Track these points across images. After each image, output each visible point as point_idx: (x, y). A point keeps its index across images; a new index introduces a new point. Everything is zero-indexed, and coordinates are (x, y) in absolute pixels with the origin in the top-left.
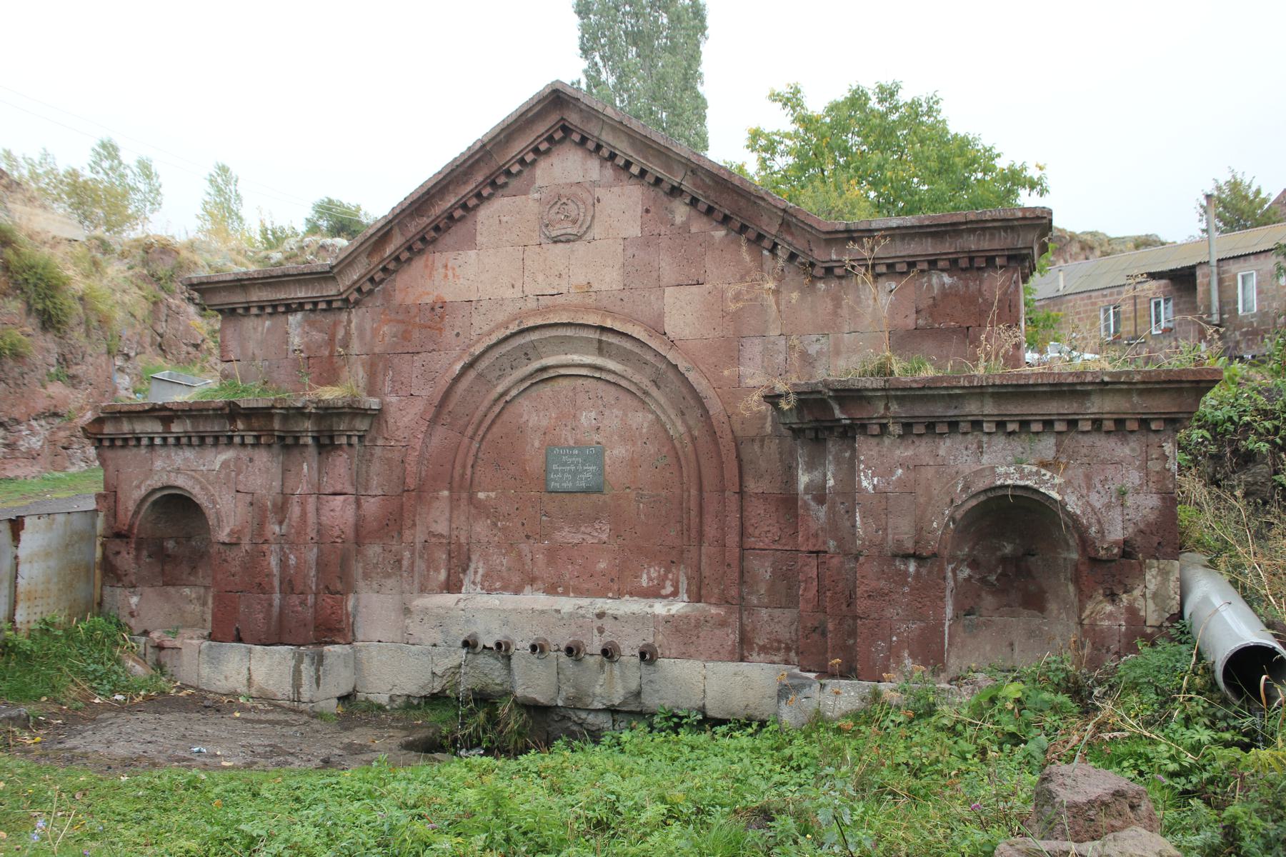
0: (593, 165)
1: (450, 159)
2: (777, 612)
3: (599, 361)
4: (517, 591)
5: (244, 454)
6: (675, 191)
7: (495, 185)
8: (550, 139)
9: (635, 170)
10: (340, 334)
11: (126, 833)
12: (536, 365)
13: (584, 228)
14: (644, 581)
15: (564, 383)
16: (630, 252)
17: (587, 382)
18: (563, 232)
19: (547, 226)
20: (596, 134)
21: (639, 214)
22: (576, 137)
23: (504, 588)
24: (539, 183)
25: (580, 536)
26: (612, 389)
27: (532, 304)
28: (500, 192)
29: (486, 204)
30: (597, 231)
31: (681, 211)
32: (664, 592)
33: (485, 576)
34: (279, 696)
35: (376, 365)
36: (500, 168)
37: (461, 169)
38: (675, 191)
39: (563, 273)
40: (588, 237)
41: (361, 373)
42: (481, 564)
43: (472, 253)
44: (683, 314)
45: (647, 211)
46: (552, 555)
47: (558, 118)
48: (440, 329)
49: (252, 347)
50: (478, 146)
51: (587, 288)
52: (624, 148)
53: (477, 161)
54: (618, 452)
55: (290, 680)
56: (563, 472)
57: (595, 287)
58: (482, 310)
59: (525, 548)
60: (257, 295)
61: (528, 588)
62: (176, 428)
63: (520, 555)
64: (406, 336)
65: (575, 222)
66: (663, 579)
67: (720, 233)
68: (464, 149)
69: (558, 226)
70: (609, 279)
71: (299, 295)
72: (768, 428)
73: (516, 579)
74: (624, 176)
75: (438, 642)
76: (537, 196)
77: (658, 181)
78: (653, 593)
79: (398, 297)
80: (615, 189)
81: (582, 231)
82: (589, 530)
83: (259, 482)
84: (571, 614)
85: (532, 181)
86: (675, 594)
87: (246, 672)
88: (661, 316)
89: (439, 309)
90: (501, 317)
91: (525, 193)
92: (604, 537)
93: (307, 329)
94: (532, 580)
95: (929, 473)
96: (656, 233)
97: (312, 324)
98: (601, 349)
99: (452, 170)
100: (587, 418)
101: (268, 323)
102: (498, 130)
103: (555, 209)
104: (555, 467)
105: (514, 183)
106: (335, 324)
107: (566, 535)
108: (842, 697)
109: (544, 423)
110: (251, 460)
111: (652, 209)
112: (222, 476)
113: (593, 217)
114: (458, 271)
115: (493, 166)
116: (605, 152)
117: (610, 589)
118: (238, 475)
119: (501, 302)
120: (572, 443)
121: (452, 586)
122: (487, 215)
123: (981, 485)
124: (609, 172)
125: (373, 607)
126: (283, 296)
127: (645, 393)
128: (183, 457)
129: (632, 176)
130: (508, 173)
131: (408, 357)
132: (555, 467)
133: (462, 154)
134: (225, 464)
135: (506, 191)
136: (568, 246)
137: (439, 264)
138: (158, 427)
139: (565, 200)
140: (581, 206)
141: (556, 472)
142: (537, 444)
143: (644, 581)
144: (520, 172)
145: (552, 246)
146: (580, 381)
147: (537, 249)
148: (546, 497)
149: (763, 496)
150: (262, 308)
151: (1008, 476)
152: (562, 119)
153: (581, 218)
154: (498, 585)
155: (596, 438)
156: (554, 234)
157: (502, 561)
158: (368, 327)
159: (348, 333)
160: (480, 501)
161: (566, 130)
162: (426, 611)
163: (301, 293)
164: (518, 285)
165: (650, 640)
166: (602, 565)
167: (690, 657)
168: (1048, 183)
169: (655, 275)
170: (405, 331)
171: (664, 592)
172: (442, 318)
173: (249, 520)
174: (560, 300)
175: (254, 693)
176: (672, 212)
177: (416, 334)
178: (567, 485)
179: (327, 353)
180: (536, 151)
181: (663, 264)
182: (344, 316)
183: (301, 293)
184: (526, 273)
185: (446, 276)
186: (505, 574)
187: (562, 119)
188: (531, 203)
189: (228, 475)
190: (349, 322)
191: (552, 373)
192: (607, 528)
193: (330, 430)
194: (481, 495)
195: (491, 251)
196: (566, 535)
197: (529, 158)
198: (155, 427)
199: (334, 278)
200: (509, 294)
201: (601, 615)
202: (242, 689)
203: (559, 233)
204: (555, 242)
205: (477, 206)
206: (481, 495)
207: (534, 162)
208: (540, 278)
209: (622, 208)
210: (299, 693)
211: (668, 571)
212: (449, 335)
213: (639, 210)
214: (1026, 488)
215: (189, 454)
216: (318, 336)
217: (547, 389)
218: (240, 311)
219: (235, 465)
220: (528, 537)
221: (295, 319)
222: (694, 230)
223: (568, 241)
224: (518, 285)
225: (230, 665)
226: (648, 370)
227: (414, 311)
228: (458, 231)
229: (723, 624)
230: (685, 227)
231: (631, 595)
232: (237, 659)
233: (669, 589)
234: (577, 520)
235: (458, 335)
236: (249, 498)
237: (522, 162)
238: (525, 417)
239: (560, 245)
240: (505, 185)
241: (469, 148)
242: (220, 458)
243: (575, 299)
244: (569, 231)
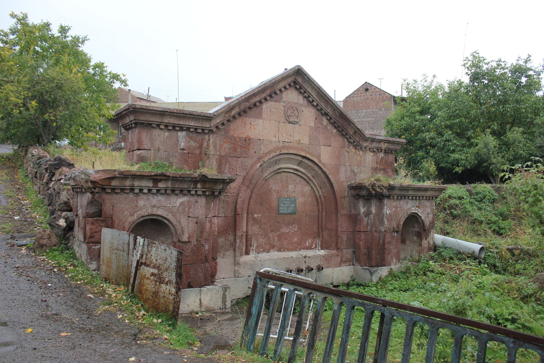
0: (301, 98)
2: (347, 250)
3: (298, 168)
4: (268, 251)
5: (193, 199)
6: (326, 114)
9: (315, 104)
10: (205, 144)
12: (278, 167)
14: (307, 244)
15: (284, 174)
16: (311, 132)
17: (292, 174)
19: (288, 117)
23: (264, 251)
24: (284, 99)
25: (289, 230)
26: (298, 178)
27: (281, 145)
31: (325, 122)
32: (313, 247)
33: (257, 247)
34: (216, 308)
35: (221, 162)
38: (326, 114)
41: (215, 163)
42: (255, 243)
43: (261, 121)
44: (325, 156)
45: (316, 119)
46: (280, 237)
48: (248, 149)
49: (157, 144)
51: (299, 142)
54: (300, 200)
55: (221, 300)
56: (284, 207)
57: (302, 142)
58: (265, 144)
59: (271, 235)
60: (167, 120)
61: (272, 250)
62: (161, 185)
63: (269, 238)
64: (235, 150)
66: (312, 243)
67: (335, 131)
70: (305, 140)
71: (191, 124)
72: (346, 194)
73: (267, 247)
74: (310, 105)
75: (251, 275)
78: (309, 248)
79: (231, 133)
82: (291, 227)
83: (201, 212)
84: (296, 258)
85: (282, 98)
86: (316, 247)
87: (199, 301)
88: (320, 155)
89: (248, 141)
90: (271, 148)
91: (279, 102)
92: (296, 230)
93: (188, 140)
94: (273, 247)
95: (399, 209)
97: (191, 138)
98: (300, 164)
100: (291, 187)
101: (167, 134)
104: (281, 205)
106: (203, 139)
107: (284, 230)
108: (383, 272)
109: (277, 188)
110: (196, 202)
112: (181, 209)
114: (255, 127)
117: (297, 248)
118: (189, 209)
119: (271, 142)
120: (286, 196)
121: (247, 253)
123: (409, 213)
124: (306, 102)
125: (224, 264)
126: (182, 123)
127: (310, 179)
128: (156, 200)
129: (313, 105)
131: (235, 159)
132: (281, 205)
134: (182, 204)
137: (248, 122)
138: (150, 184)
141: (282, 207)
142: (275, 196)
143: (307, 244)
145: (288, 124)
146: (289, 174)
148: (278, 216)
149: (344, 215)
150: (166, 126)
151: (414, 210)
154: (261, 250)
155: (294, 195)
156: (291, 120)
157: (262, 241)
158: (218, 143)
159: (208, 145)
160: (255, 218)
162: (246, 263)
163: (192, 123)
164: (277, 136)
165: (319, 264)
166: (295, 240)
167: (329, 267)
168: (128, 82)
170: (234, 148)
171: (313, 247)
172: (249, 144)
173: (196, 230)
174: (291, 145)
175: (203, 309)
177: (239, 150)
178: (285, 212)
179: (198, 152)
180: (285, 88)
182: (207, 137)
183: (192, 123)
185: (251, 128)
186: (264, 246)
189: (184, 209)
190: (209, 140)
191: (281, 170)
192: (296, 227)
193: (212, 188)
194: (256, 216)
195: (268, 121)
196: (284, 230)
198: (147, 184)
199: (211, 120)
200: (274, 139)
201: (305, 257)
202: (196, 309)
206: (256, 216)
208: (284, 135)
209: (309, 115)
210: (225, 305)
211: (314, 240)
212: (252, 152)
214: (416, 213)
215: (161, 198)
216: (193, 144)
217: (278, 176)
218: (155, 126)
219: (188, 204)
220: (272, 231)
221: (182, 135)
222: (328, 128)
223: (294, 124)
224: (277, 136)
225: (190, 299)
226: (313, 173)
227: (238, 140)
228: (255, 111)
229: (338, 255)
230: (326, 127)
231: (304, 249)
232: (194, 296)
233: (314, 246)
234: (289, 224)
235: (255, 152)
236: (195, 220)
238: (271, 186)
239: (291, 124)
242: (179, 201)
243: (296, 145)
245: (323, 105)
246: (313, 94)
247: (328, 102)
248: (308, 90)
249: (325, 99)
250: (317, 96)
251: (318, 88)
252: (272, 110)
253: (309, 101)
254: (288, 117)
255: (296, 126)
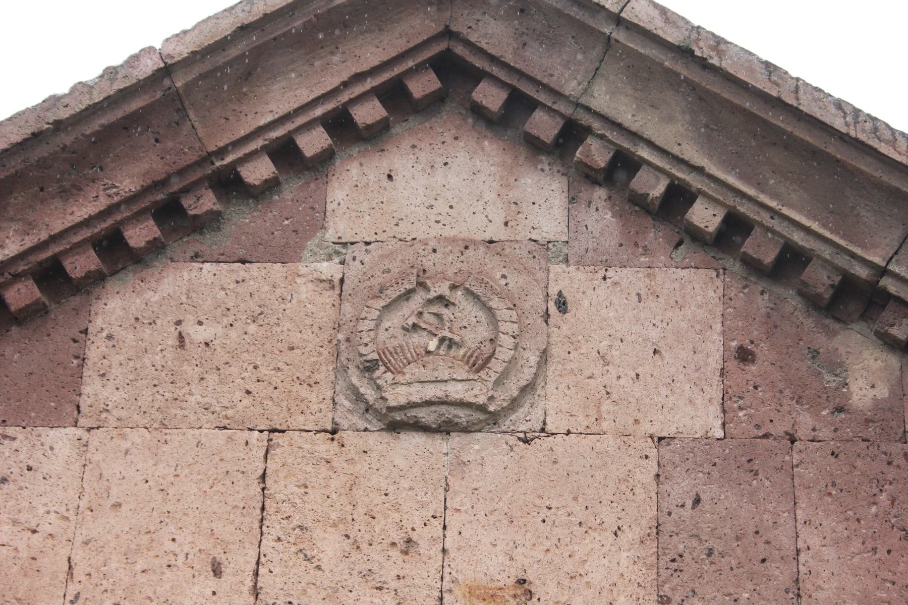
0: (543, 202)
1: (34, 98)
7: (178, 217)
8: (394, 95)
9: (705, 216)
11: (214, 402)
13: (512, 389)
16: (681, 487)
18: (432, 392)
19: (369, 367)
20: (571, 88)
21: (715, 361)
22: (490, 97)
24: (339, 226)
28: (194, 244)
29: (130, 278)
30: (555, 404)
36: (208, 158)
37: (66, 139)
39: (422, 536)
40: (526, 418)
43: (61, 439)
45: (744, 356)
47: (433, 28)
50: (149, 66)
52: (669, 133)
53: (126, 125)
65: (478, 364)
68: (90, 72)
69: (414, 371)
74: (656, 236)
76: (329, 269)
77: (790, 262)
80: (626, 276)
81: (503, 397)
91: (285, 254)
96: (779, 428)
99: (37, 137)
102: (227, 27)
103: (406, 313)
105: (244, 220)
111: (763, 351)
113: (544, 356)
115: (180, 150)
116: (596, 153)
122: (131, 322)
124: (601, 219)
130: (229, 184)
133: (81, 88)
135: (208, 242)
136: (439, 444)
139: (443, 289)
140: (503, 313)
144: (271, 186)
145: (378, 441)
147: (323, 446)
152: (448, 33)
153: (504, 354)
156: (397, 396)
161: (456, 70)
164: (240, 563)
169: (781, 574)
176: (836, 366)
180: (340, 125)
181: (810, 538)
184: (274, 527)
187: (448, 33)
188: (305, 290)
197: (313, 142)
203: (416, 394)
204: (394, 427)
205: (96, 279)
207: (326, 158)
208: (329, 546)
213: (714, 351)
223: (446, 428)
237: (285, 153)
239: (413, 441)
240: (212, 221)
241: (111, 73)
244: (457, 391)
245: (792, 212)
246: (669, 133)
247: (850, 173)
248: (602, 99)
249: (790, 144)
250: (709, 143)
251: (684, 52)
252: (197, 334)
253: (639, 202)
254: (369, 367)
255: (479, 446)
